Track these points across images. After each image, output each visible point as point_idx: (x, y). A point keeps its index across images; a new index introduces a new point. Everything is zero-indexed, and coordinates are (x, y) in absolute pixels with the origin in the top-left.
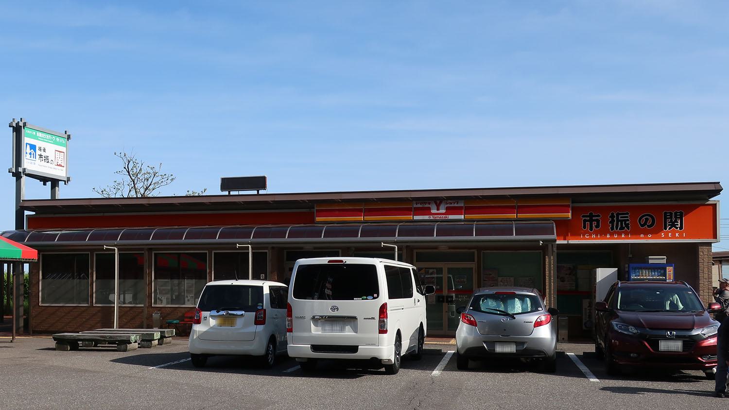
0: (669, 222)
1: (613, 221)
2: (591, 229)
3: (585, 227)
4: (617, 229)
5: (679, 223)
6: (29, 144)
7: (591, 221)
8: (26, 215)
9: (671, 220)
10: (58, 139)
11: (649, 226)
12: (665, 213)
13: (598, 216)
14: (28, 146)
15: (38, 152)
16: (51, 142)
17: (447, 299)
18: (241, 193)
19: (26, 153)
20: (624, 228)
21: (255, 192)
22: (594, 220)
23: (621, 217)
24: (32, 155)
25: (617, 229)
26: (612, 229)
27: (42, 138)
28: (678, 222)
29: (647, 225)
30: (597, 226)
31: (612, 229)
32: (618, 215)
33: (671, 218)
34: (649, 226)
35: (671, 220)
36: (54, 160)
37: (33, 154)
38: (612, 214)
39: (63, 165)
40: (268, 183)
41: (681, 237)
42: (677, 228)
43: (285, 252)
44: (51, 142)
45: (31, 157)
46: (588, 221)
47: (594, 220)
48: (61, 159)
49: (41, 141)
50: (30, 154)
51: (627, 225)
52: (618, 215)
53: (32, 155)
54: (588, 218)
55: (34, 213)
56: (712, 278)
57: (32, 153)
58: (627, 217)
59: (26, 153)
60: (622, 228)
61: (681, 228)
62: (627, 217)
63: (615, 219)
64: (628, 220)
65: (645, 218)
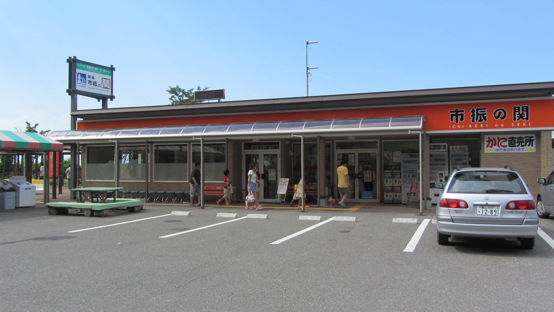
0: (517, 115)
1: (473, 116)
2: (457, 121)
3: (452, 120)
4: (477, 121)
5: (525, 115)
6: (80, 73)
7: (457, 115)
8: (377, 148)
9: (519, 113)
10: (104, 71)
11: (502, 118)
12: (515, 108)
13: (462, 111)
14: (79, 76)
15: (88, 79)
16: (98, 72)
17: (355, 176)
18: (210, 101)
19: (78, 79)
20: (482, 120)
21: (217, 101)
22: (460, 115)
23: (480, 112)
24: (83, 81)
25: (477, 121)
26: (473, 121)
27: (91, 70)
28: (525, 114)
29: (501, 118)
30: (462, 119)
31: (473, 121)
32: (477, 110)
33: (519, 111)
34: (502, 118)
35: (519, 113)
36: (101, 84)
37: (84, 80)
38: (473, 109)
39: (109, 88)
40: (226, 94)
41: (527, 126)
42: (524, 119)
43: (243, 143)
44: (98, 72)
45: (81, 82)
46: (454, 115)
47: (460, 115)
48: (107, 84)
49: (91, 71)
50: (81, 80)
51: (485, 118)
52: (477, 110)
53: (83, 81)
54: (455, 113)
55: (82, 119)
56: (18, 175)
57: (83, 79)
58: (485, 111)
59: (78, 79)
60: (481, 120)
61: (527, 119)
62: (485, 111)
63: (475, 113)
64: (485, 114)
65: (499, 112)
